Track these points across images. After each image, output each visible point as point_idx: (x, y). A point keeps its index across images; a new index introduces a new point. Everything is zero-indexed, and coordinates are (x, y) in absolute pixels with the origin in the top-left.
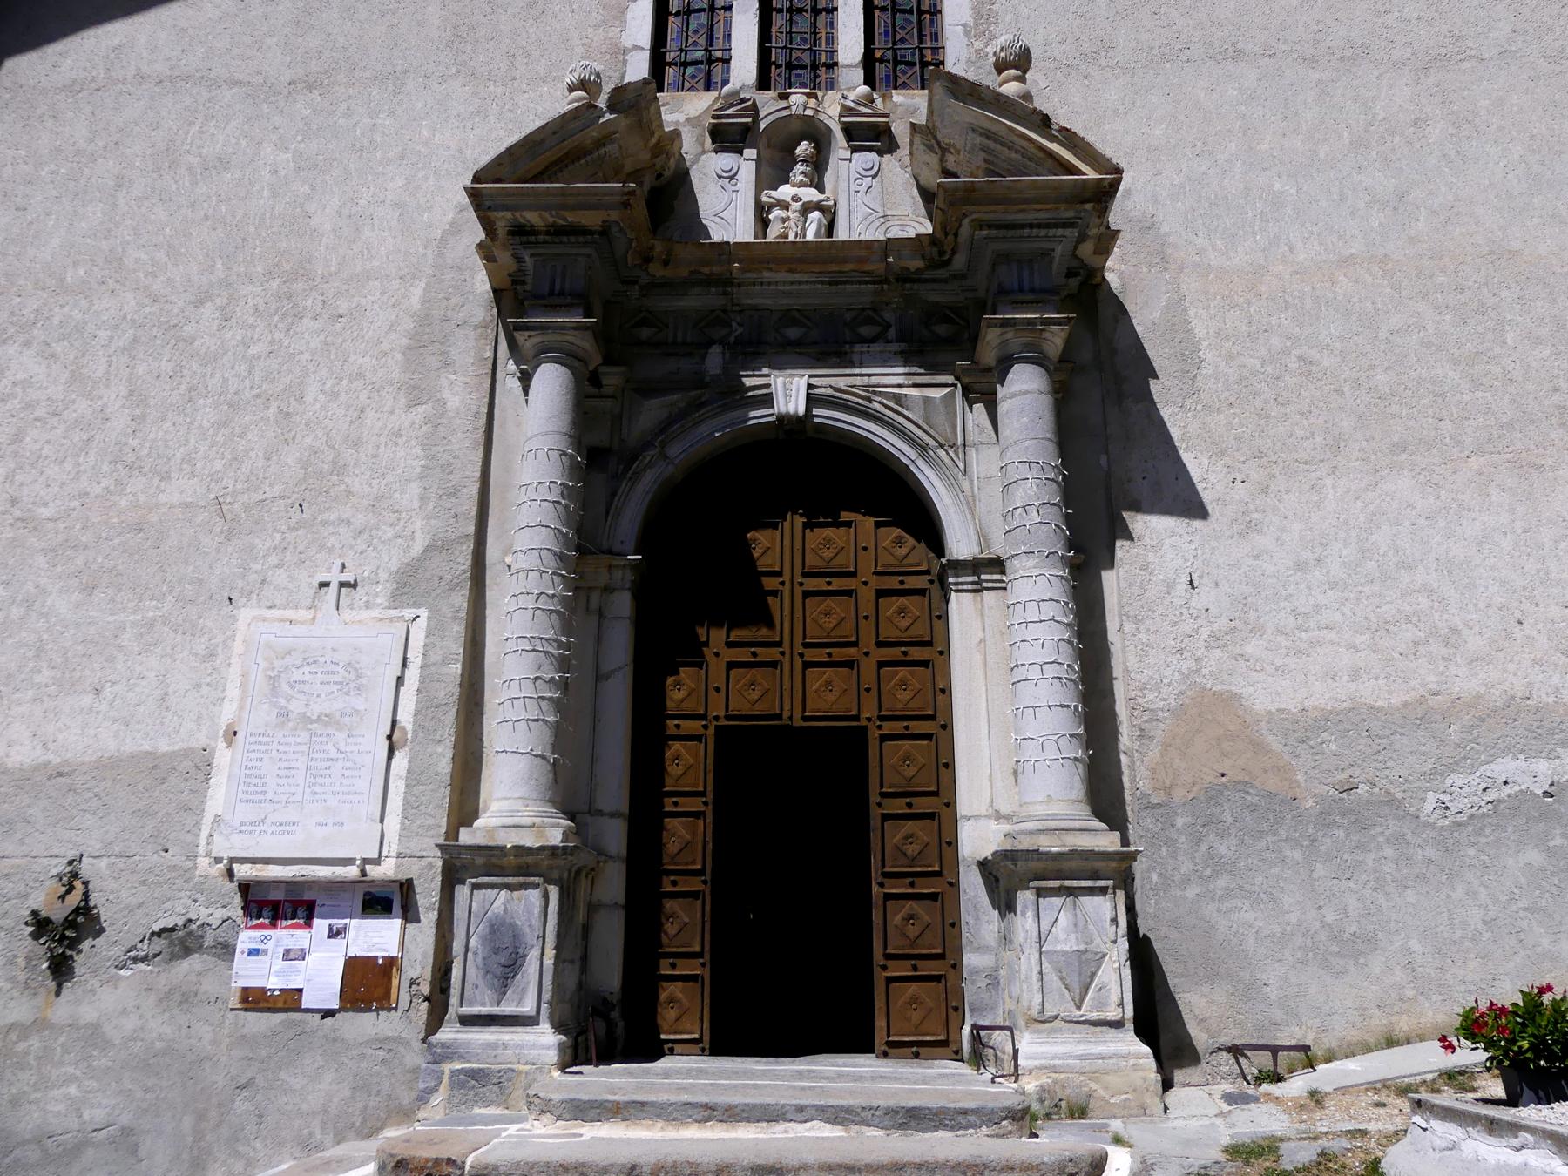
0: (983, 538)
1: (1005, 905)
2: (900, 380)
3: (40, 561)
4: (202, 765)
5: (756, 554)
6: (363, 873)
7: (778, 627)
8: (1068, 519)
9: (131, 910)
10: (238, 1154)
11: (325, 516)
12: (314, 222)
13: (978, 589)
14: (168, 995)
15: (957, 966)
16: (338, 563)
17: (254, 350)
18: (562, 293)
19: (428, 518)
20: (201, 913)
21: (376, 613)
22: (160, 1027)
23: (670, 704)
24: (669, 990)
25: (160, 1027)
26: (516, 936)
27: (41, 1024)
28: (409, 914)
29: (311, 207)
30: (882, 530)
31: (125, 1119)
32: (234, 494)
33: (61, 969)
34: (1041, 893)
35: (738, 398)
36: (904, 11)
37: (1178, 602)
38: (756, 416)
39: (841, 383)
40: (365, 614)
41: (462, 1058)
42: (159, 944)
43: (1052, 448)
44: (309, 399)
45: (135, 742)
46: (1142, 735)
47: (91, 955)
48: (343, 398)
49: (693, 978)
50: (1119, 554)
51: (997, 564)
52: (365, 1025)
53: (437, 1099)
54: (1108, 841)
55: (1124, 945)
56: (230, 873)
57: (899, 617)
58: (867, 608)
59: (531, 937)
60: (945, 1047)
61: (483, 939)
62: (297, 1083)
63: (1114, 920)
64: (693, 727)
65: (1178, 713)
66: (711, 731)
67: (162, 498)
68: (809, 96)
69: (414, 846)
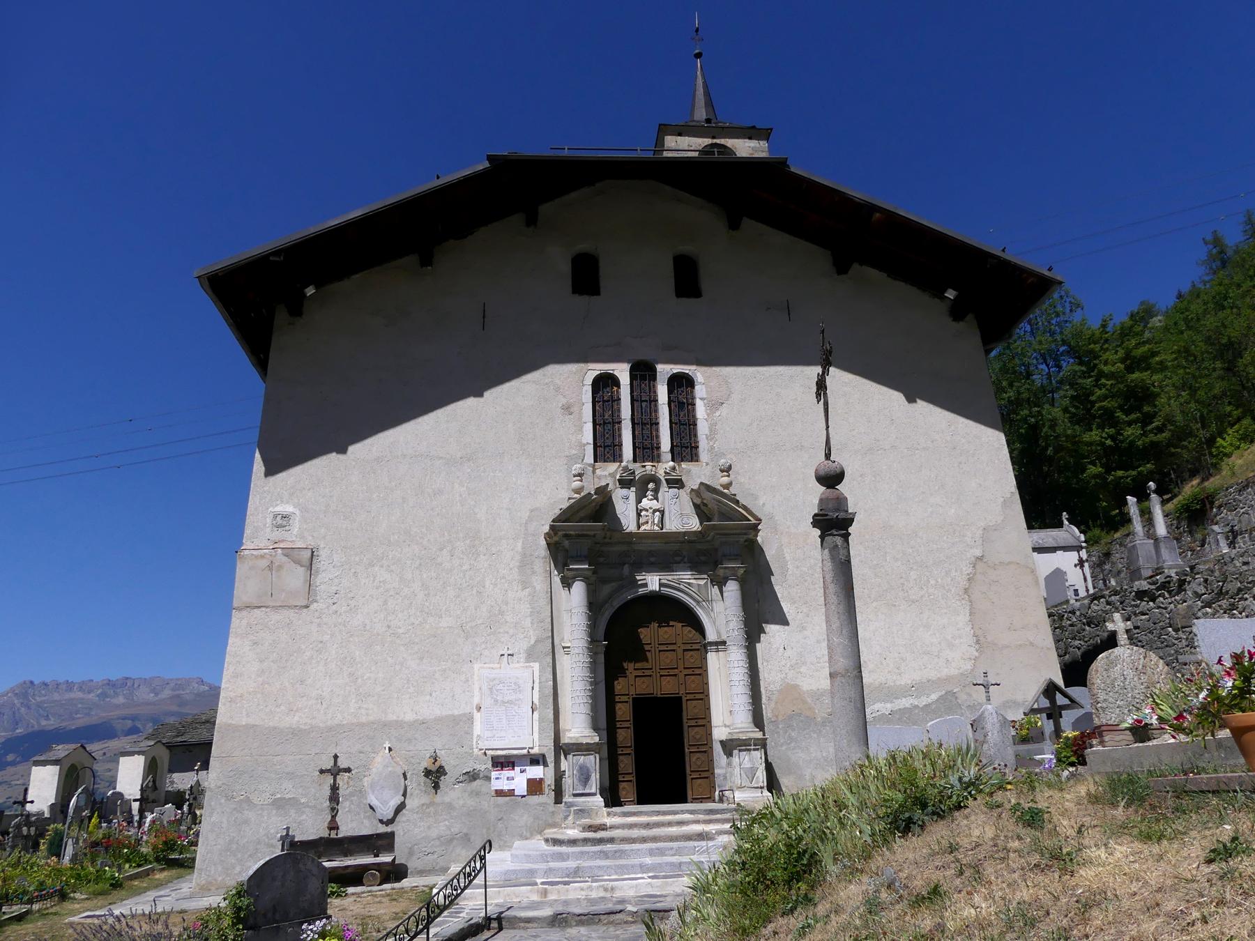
0: (718, 633)
1: (729, 754)
2: (690, 577)
3: (402, 648)
4: (470, 719)
5: (642, 637)
6: (529, 752)
7: (650, 661)
8: (746, 633)
9: (455, 767)
10: (501, 840)
11: (499, 630)
12: (478, 516)
13: (718, 651)
14: (472, 792)
15: (713, 774)
16: (506, 648)
17: (464, 568)
18: (580, 556)
19: (534, 630)
20: (478, 767)
21: (521, 664)
22: (471, 802)
23: (616, 690)
24: (622, 785)
25: (471, 802)
26: (588, 770)
27: (432, 804)
28: (545, 765)
29: (477, 510)
30: (684, 628)
31: (465, 831)
32: (466, 623)
33: (436, 787)
34: (740, 751)
35: (634, 584)
36: (684, 424)
37: (780, 654)
38: (641, 591)
39: (670, 578)
40: (517, 665)
41: (576, 806)
42: (466, 777)
43: (741, 609)
44: (487, 586)
45: (446, 712)
46: (769, 699)
47: (444, 781)
48: (499, 586)
49: (631, 781)
50: (762, 639)
51: (724, 643)
52: (535, 799)
53: (570, 818)
54: (759, 735)
55: (764, 765)
56: (485, 754)
57: (691, 658)
58: (680, 656)
59: (592, 770)
60: (710, 799)
61: (578, 771)
62: (517, 818)
63: (761, 758)
64: (625, 698)
65: (780, 691)
66: (631, 699)
67: (441, 625)
68: (653, 466)
69: (544, 742)
